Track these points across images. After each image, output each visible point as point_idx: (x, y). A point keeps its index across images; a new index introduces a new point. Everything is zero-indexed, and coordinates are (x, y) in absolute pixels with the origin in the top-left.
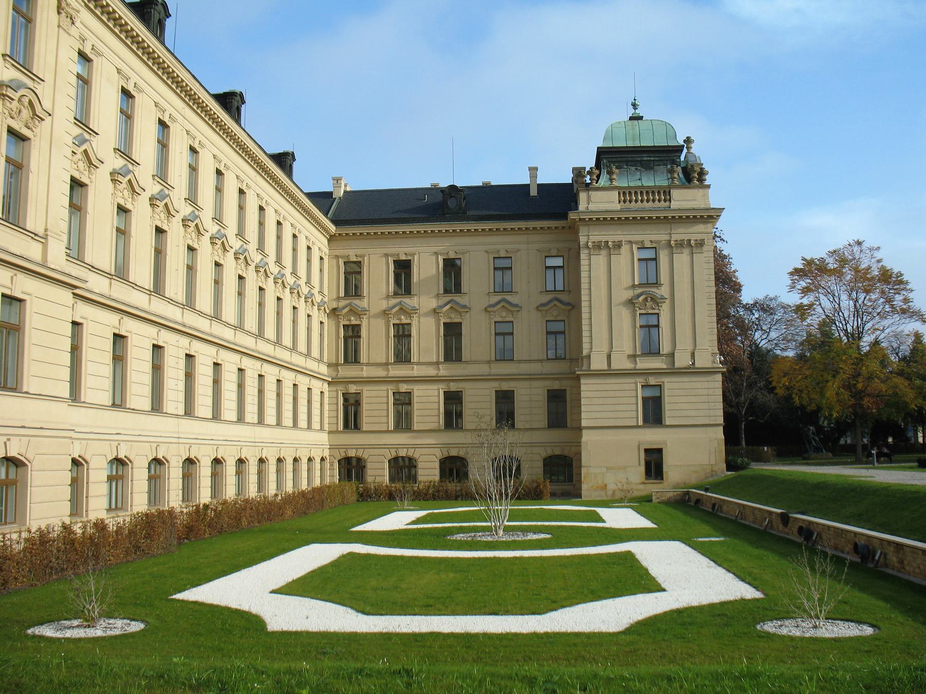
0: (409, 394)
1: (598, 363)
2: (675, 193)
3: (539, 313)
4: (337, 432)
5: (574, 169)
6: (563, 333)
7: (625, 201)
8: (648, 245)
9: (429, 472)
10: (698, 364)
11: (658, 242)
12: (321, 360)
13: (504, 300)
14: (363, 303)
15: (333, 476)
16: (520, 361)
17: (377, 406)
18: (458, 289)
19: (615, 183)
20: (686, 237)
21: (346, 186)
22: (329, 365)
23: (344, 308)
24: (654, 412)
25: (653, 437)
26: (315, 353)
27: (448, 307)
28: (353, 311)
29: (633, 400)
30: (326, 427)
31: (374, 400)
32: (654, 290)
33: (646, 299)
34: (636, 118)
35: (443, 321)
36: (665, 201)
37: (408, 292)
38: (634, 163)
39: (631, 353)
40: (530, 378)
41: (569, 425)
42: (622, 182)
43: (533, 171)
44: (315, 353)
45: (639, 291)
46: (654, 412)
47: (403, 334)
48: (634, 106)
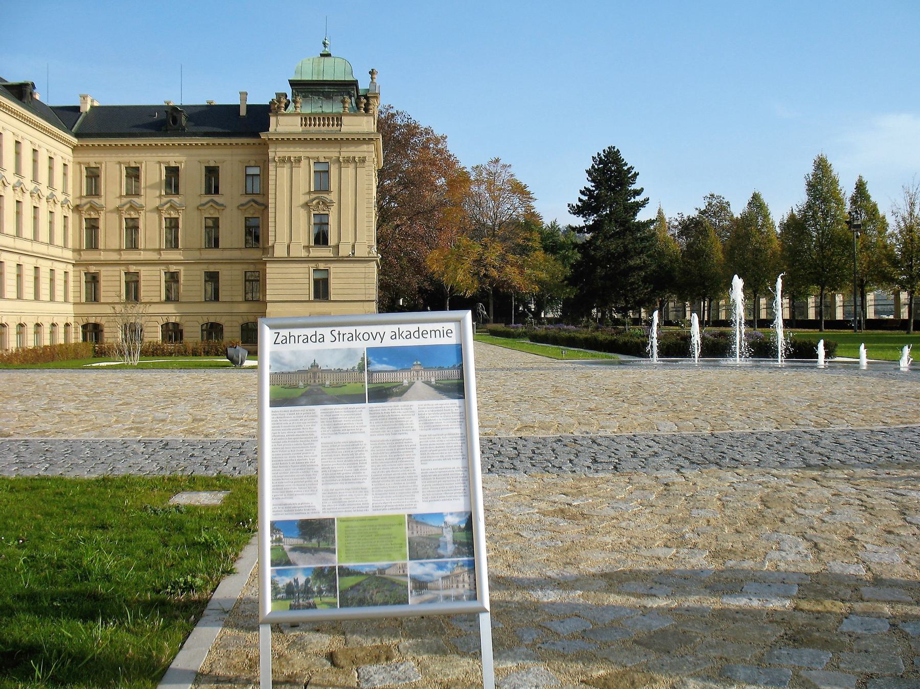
0: (137, 274)
1: (280, 251)
2: (345, 119)
8: (322, 160)
9: (193, 335)
11: (330, 158)
12: (65, 246)
14: (101, 201)
15: (76, 337)
16: (224, 249)
17: (112, 284)
18: (97, 195)
19: (298, 111)
21: (92, 101)
22: (74, 251)
23: (85, 205)
26: (59, 239)
27: (168, 205)
28: (93, 208)
29: (307, 281)
30: (71, 299)
31: (109, 278)
32: (325, 195)
33: (318, 203)
37: (138, 195)
38: (317, 93)
40: (231, 262)
42: (307, 109)
43: (244, 95)
44: (59, 239)
45: (314, 196)
47: (133, 227)
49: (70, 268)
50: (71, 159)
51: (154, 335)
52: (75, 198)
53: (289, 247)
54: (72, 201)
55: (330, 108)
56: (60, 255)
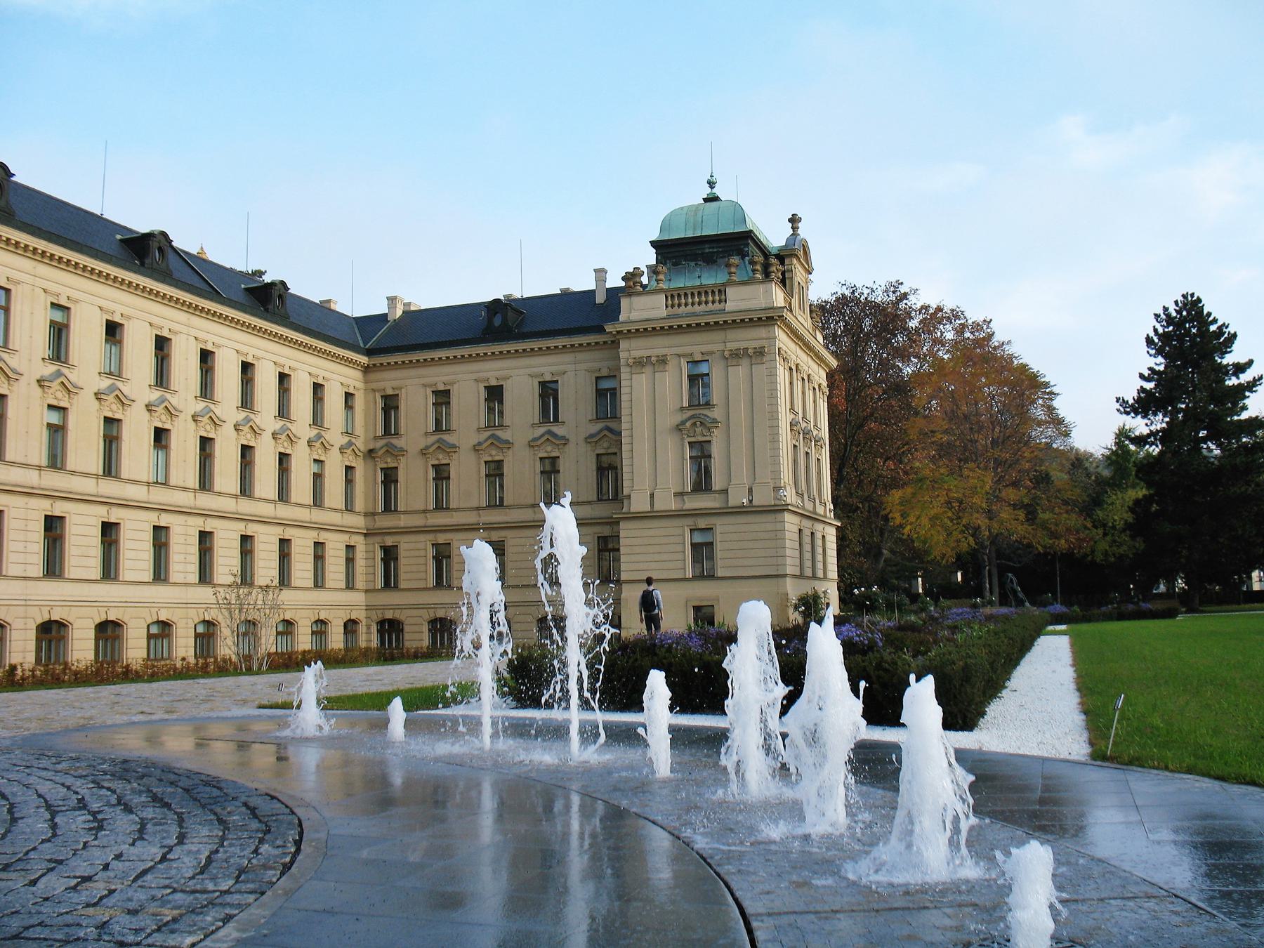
1: (639, 503)
2: (731, 291)
4: (374, 590)
7: (673, 306)
10: (657, 507)
13: (550, 432)
19: (661, 285)
20: (743, 345)
22: (366, 515)
31: (412, 553)
32: (705, 412)
33: (695, 424)
34: (712, 199)
35: (687, 440)
36: (720, 301)
38: (694, 257)
39: (679, 490)
43: (600, 274)
48: (711, 184)
49: (358, 541)
50: (360, 385)
51: (416, 636)
52: (366, 442)
53: (652, 496)
54: (360, 444)
55: (710, 278)
56: (339, 523)
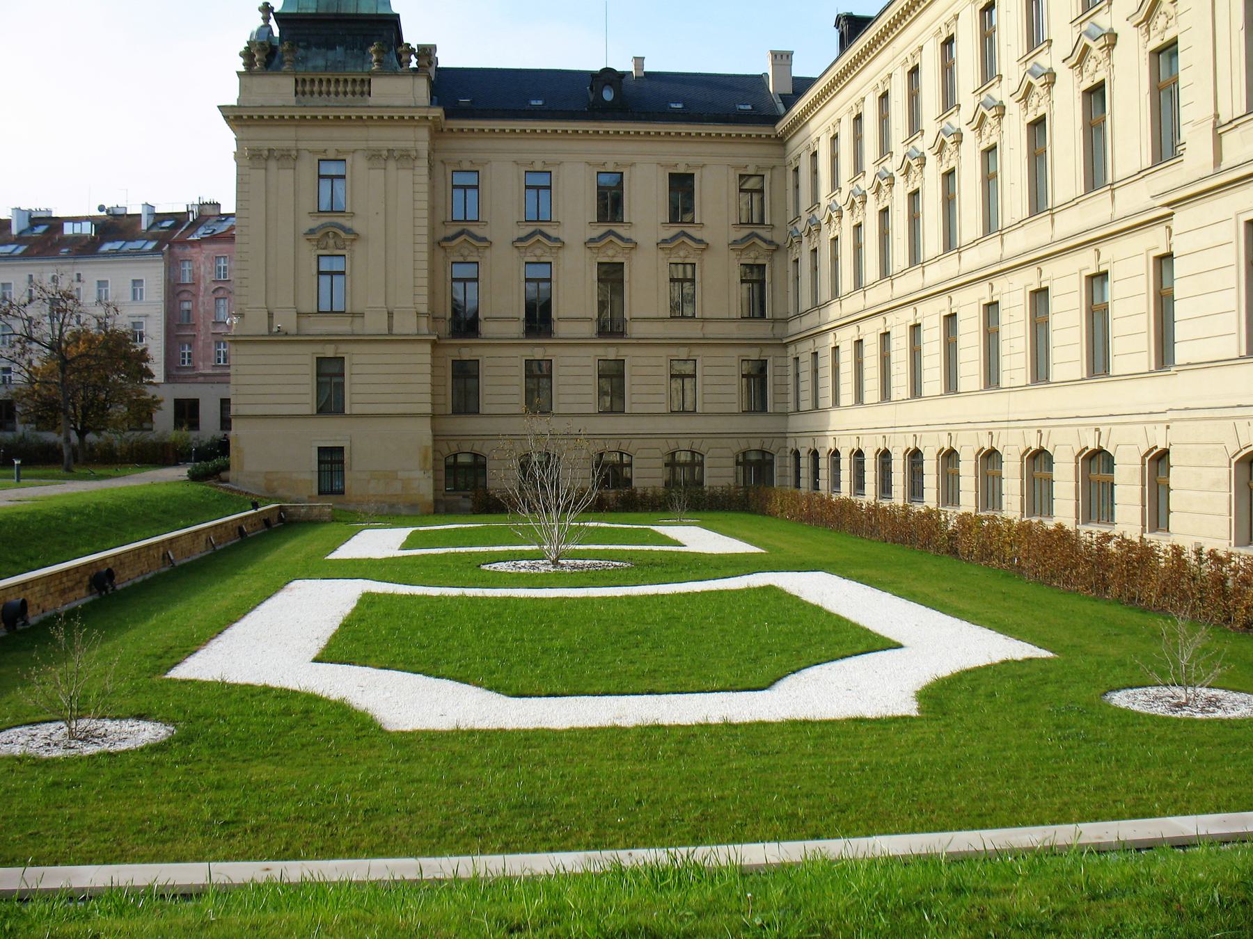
3: (516, 251)
5: (435, 47)
6: (343, 273)
13: (610, 233)
24: (330, 398)
25: (331, 432)
41: (347, 411)
43: (639, 61)
46: (330, 398)
